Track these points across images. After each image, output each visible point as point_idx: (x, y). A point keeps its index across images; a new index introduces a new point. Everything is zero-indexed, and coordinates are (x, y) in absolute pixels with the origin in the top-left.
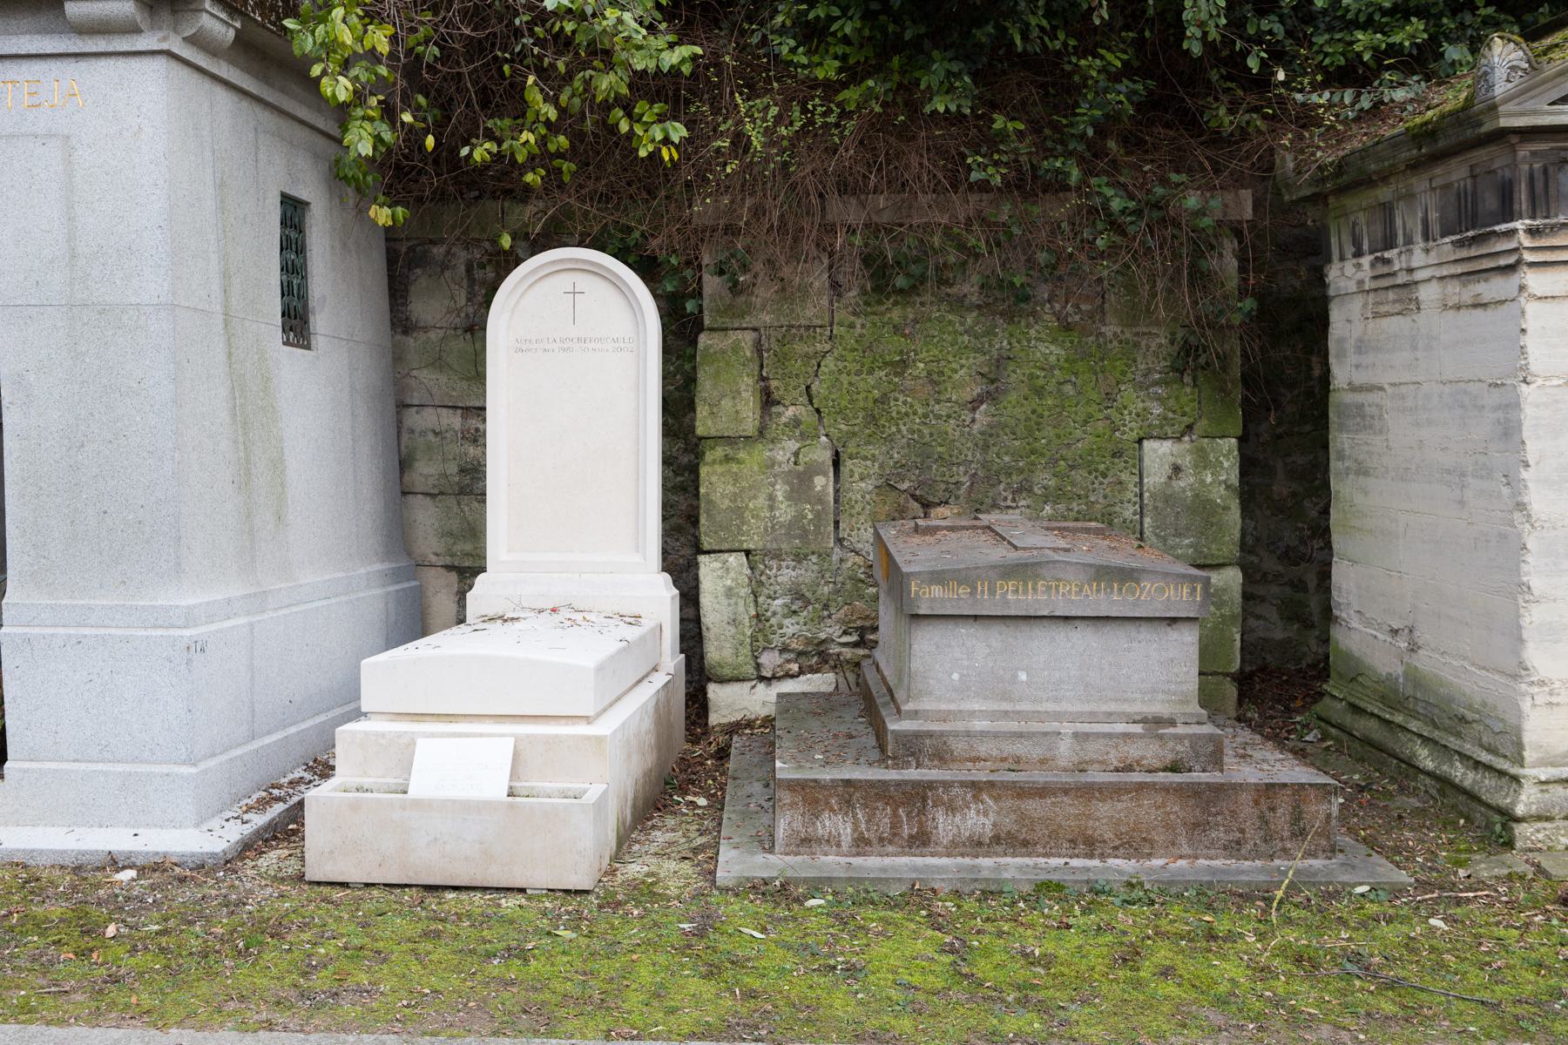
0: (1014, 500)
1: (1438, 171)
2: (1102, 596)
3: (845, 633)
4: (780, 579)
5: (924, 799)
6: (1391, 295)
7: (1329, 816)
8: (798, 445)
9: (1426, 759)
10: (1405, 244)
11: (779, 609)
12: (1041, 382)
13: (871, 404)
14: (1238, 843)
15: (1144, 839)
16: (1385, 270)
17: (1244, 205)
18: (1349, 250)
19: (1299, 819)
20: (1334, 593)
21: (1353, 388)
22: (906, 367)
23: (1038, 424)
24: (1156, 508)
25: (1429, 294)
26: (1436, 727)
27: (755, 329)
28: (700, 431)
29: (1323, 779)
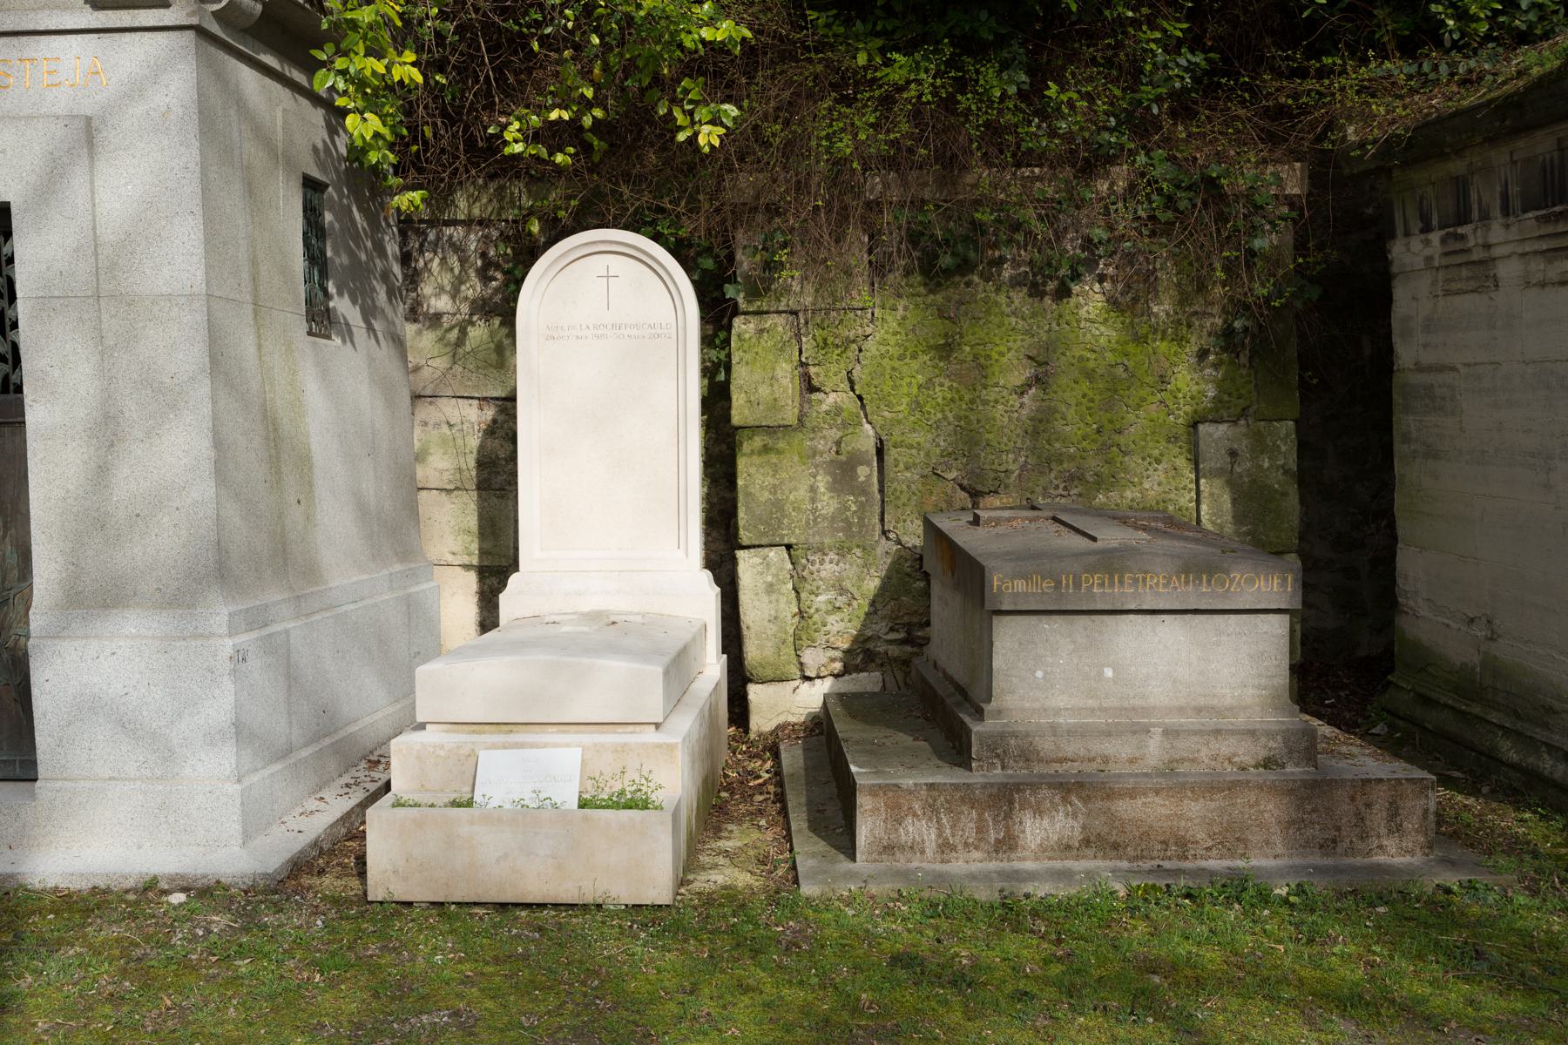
0: (1065, 488)
1: (1521, 143)
2: (1191, 588)
3: (892, 630)
4: (823, 574)
5: (1011, 802)
6: (1465, 272)
7: (1426, 811)
8: (840, 434)
9: (1509, 751)
10: (1480, 220)
11: (823, 607)
12: (1091, 364)
13: (915, 390)
14: (1334, 841)
15: (1238, 839)
16: (1458, 246)
17: (1293, 180)
18: (1415, 225)
19: (1396, 814)
20: (1400, 581)
21: (1420, 368)
22: (952, 350)
23: (1089, 408)
24: (1212, 494)
25: (1508, 270)
26: (1519, 717)
27: (795, 313)
28: (736, 419)
29: (1419, 774)
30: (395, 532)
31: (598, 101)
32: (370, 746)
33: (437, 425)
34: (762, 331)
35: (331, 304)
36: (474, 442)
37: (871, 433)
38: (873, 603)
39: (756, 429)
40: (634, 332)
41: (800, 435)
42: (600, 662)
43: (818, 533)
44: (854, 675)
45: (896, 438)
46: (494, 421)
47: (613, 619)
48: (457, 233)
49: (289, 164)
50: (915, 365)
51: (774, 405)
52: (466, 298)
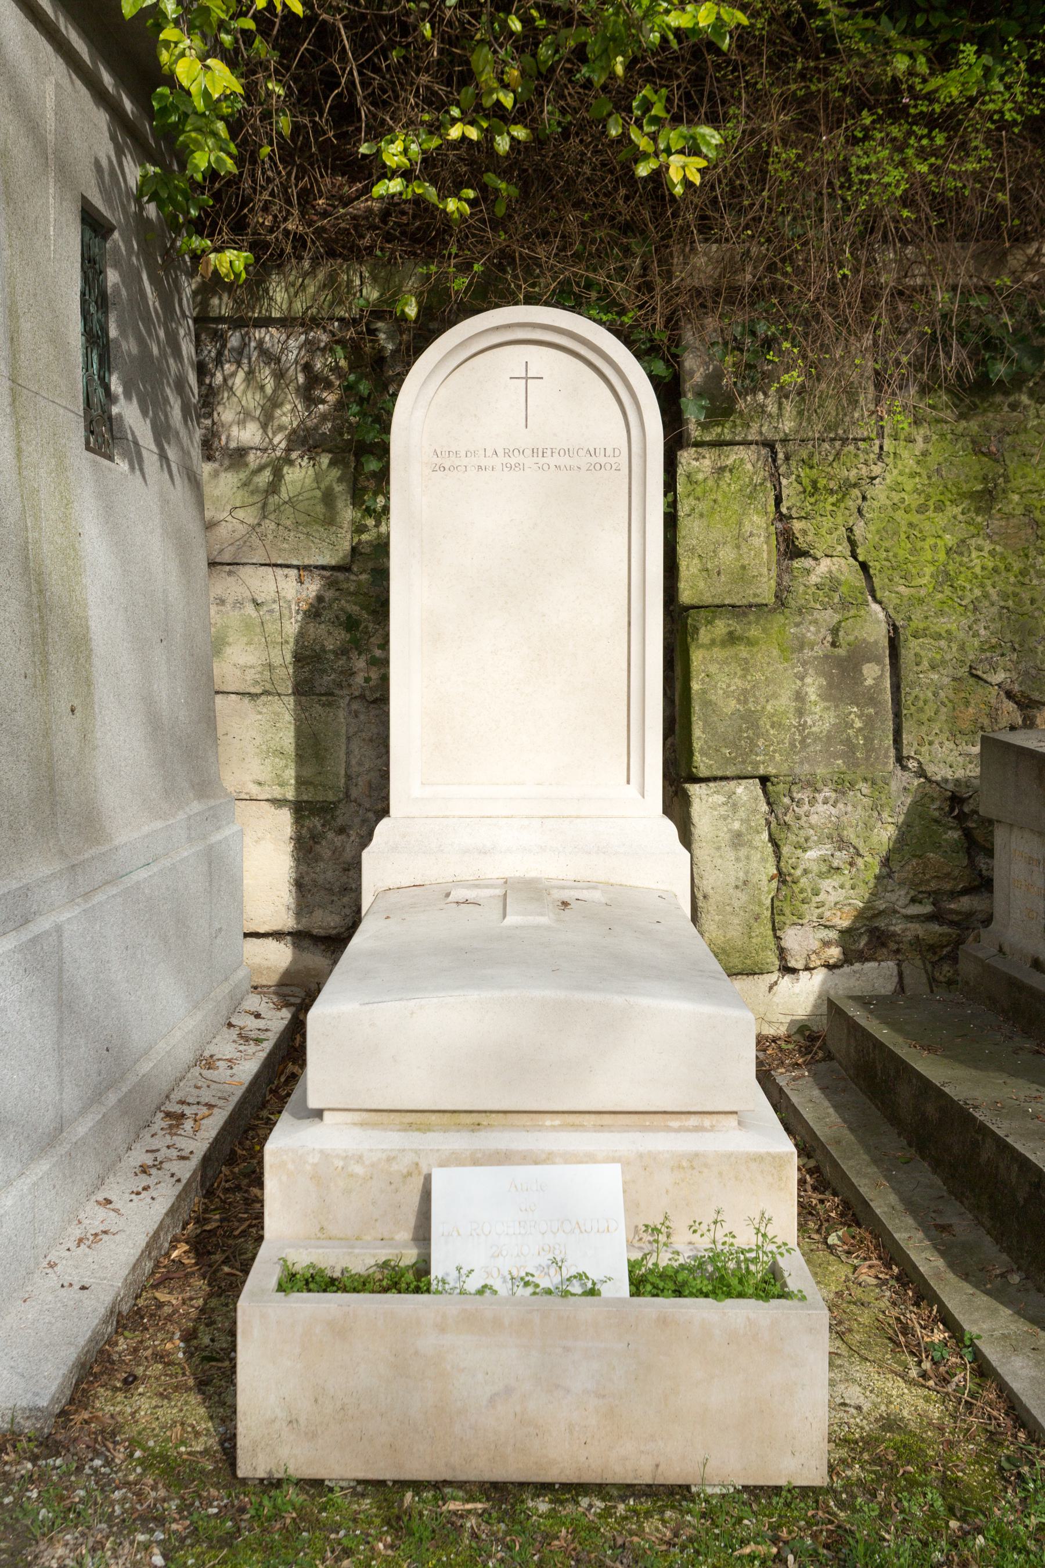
3: (913, 900)
4: (814, 819)
8: (837, 617)
11: (815, 868)
13: (942, 556)
30: (189, 758)
31: (522, 114)
32: (165, 1087)
33: (239, 604)
34: (722, 469)
35: (115, 410)
36: (292, 628)
37: (881, 615)
38: (886, 862)
39: (717, 609)
40: (565, 461)
41: (781, 619)
42: (644, 1002)
43: (807, 759)
44: (857, 966)
45: (917, 623)
46: (320, 599)
47: (565, 895)
48: (271, 337)
49: (64, 173)
50: (941, 520)
51: (742, 575)
52: (281, 428)
